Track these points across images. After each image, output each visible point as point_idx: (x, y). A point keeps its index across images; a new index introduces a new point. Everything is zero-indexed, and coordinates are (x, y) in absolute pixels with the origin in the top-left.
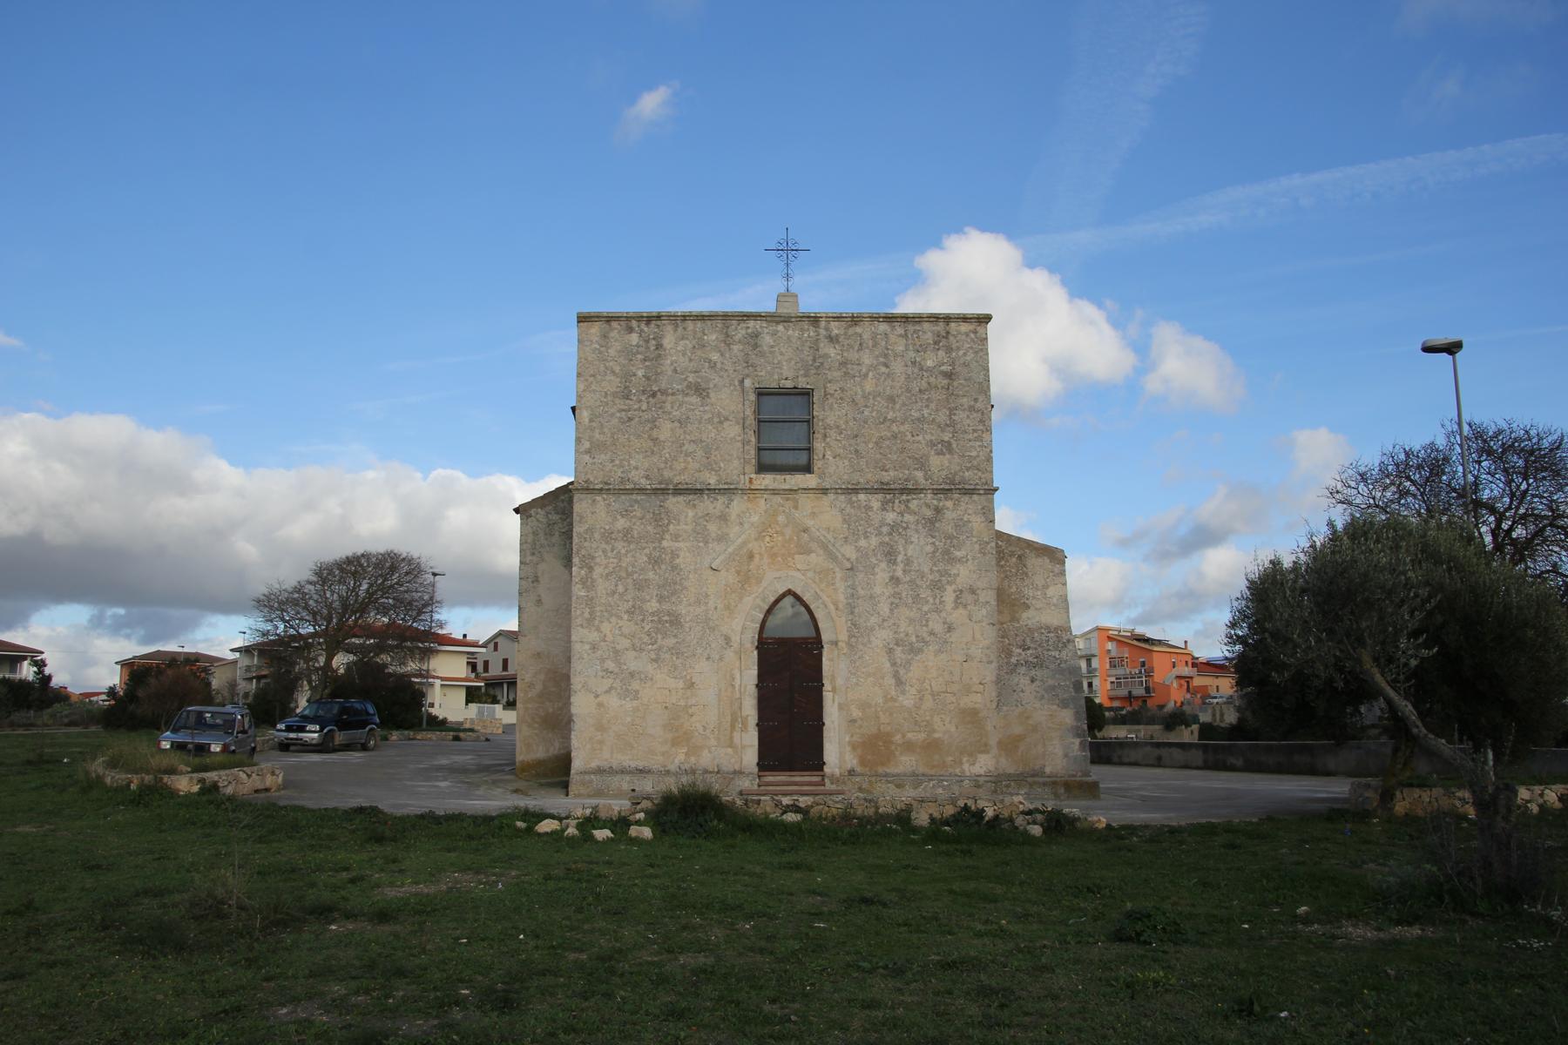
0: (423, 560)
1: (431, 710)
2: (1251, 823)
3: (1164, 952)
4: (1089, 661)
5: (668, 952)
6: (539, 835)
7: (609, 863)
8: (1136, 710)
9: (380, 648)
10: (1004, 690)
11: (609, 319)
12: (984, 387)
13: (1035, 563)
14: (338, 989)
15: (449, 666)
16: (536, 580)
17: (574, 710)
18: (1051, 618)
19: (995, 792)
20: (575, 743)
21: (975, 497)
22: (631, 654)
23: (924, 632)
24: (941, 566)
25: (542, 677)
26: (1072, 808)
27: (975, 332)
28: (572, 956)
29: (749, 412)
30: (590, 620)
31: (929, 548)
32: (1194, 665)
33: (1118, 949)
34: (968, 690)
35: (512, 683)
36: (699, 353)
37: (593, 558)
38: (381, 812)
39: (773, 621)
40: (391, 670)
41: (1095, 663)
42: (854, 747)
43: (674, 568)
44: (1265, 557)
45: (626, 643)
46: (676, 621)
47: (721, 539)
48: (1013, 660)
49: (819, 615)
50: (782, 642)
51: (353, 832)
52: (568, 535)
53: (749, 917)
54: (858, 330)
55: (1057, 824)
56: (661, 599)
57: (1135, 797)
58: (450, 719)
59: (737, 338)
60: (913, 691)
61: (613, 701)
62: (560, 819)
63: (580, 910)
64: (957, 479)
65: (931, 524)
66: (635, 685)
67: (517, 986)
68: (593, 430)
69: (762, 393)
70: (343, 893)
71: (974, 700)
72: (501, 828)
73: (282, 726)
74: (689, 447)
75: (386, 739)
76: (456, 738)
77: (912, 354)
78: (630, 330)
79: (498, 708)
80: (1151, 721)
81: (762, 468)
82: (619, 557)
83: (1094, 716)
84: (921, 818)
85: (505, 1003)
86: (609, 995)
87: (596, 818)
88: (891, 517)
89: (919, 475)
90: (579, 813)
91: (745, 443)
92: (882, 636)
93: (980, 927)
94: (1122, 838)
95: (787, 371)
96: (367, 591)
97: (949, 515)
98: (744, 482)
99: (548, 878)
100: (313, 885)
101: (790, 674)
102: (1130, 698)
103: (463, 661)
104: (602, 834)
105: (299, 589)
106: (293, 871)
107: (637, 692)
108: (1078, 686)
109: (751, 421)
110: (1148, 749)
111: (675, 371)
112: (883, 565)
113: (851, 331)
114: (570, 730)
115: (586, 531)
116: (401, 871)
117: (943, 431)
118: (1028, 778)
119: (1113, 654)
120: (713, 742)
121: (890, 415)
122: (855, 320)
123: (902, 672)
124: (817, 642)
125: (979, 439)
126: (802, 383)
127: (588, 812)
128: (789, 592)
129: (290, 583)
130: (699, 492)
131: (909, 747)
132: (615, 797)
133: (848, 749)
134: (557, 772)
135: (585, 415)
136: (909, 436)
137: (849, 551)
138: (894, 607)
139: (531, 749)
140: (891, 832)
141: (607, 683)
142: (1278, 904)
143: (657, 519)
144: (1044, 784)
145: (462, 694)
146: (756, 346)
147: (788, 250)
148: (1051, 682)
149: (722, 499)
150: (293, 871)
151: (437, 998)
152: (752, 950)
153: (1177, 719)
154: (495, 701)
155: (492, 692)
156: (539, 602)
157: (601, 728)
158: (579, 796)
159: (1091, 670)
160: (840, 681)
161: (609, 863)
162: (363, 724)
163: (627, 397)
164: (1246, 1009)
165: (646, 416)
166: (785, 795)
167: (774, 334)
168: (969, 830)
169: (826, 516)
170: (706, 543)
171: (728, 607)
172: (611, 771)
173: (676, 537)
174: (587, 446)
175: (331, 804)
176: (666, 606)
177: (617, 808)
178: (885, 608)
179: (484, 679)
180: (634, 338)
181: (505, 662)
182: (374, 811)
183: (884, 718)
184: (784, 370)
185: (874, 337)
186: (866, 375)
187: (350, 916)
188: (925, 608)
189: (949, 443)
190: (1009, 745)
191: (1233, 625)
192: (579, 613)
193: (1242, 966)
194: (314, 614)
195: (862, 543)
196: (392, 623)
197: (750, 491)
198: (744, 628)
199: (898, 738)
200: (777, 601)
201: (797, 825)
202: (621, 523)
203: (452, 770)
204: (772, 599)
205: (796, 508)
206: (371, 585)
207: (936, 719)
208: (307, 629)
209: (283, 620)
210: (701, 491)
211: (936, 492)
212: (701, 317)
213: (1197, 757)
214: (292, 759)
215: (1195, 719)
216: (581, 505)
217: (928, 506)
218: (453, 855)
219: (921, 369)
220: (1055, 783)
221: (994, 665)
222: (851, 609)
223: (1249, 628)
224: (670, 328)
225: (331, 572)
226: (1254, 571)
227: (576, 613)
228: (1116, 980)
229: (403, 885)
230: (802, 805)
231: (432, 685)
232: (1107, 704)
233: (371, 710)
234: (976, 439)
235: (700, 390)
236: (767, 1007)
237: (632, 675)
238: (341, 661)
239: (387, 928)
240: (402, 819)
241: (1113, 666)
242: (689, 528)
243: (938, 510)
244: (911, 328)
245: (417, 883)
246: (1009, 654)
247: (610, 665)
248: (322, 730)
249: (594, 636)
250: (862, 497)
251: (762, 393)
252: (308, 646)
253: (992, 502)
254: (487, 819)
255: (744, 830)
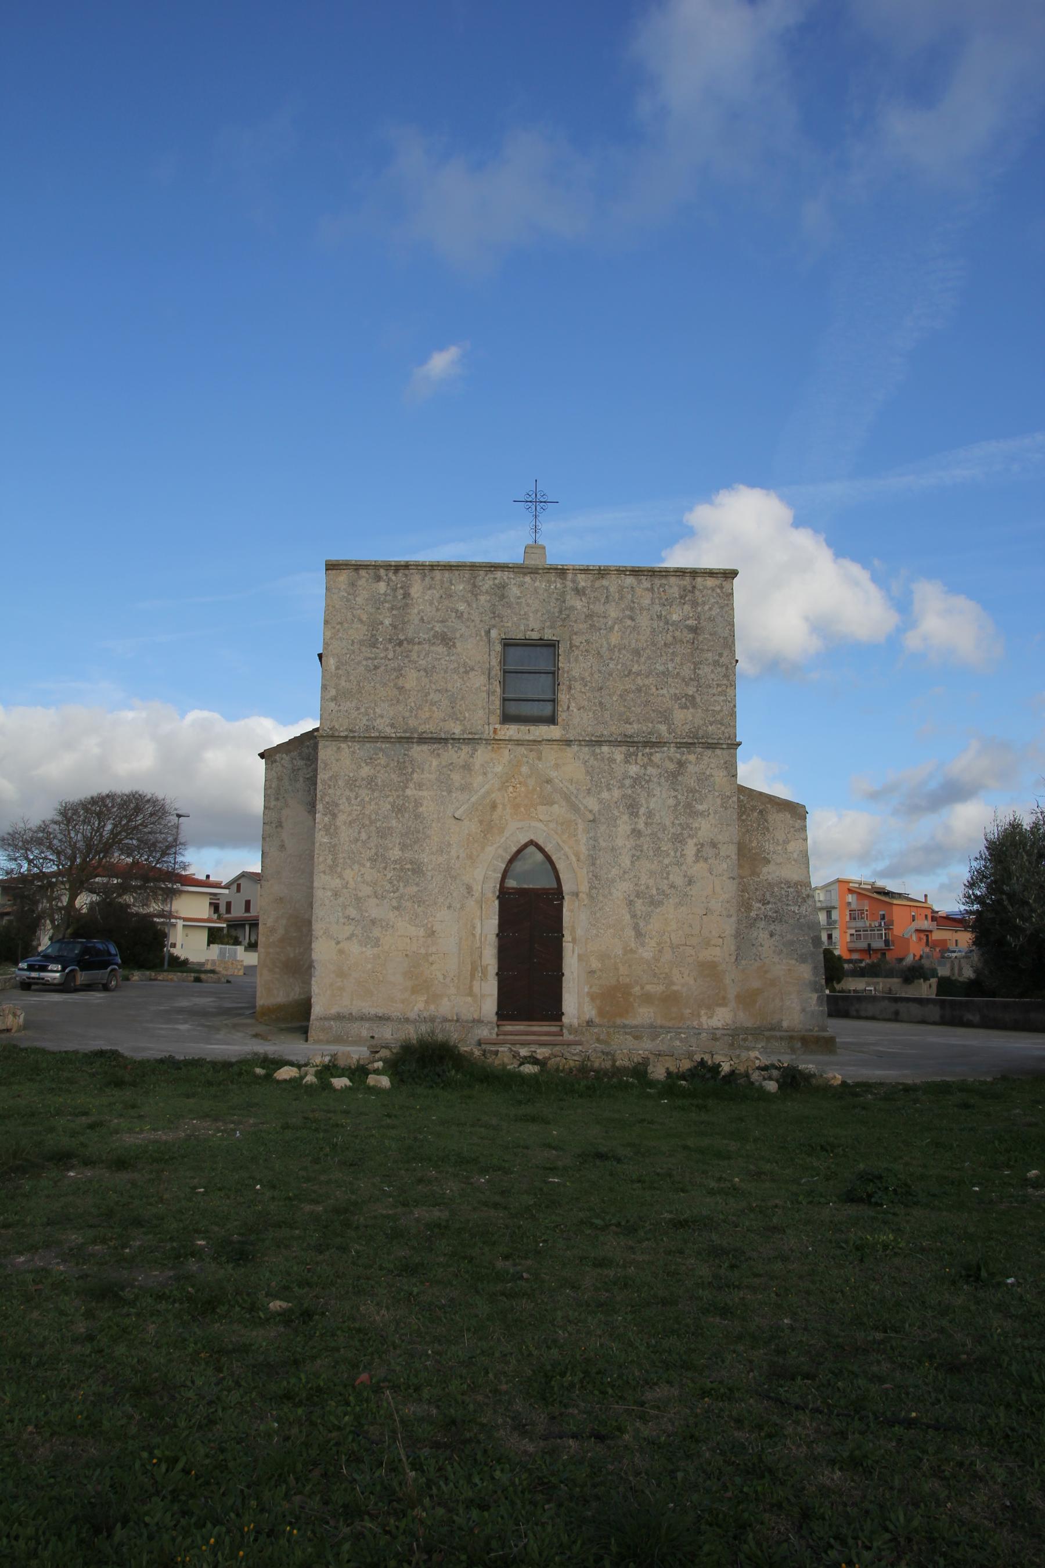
0: (168, 801)
1: (172, 950)
2: (985, 1083)
3: (894, 1214)
4: (829, 912)
5: (404, 1205)
6: (278, 1082)
7: (346, 1112)
8: (876, 962)
9: (124, 889)
10: (743, 942)
11: (357, 567)
12: (729, 643)
13: (776, 818)
14: (75, 1238)
15: (192, 907)
16: (280, 825)
17: (315, 956)
18: (790, 873)
19: (732, 1045)
20: (315, 989)
21: (718, 752)
22: (373, 901)
23: (664, 885)
24: (682, 819)
25: (284, 922)
26: (808, 1065)
27: (721, 587)
28: (308, 1208)
29: (495, 662)
30: (332, 868)
31: (671, 802)
32: (933, 919)
33: (852, 1210)
34: (707, 943)
35: (254, 925)
36: (446, 602)
37: (337, 805)
38: (122, 1056)
39: (519, 866)
40: (134, 910)
41: (835, 915)
42: (593, 998)
43: (417, 816)
44: (1005, 818)
45: (366, 890)
46: (418, 870)
47: (465, 788)
48: (753, 914)
49: (560, 866)
50: (522, 892)
51: (93, 1075)
52: (312, 781)
53: (483, 1171)
54: (605, 582)
55: (792, 1080)
56: (404, 847)
57: (876, 1052)
58: (191, 959)
59: (484, 589)
60: (653, 943)
61: (354, 948)
62: (299, 1067)
63: (316, 1161)
64: (701, 733)
65: (674, 777)
66: (376, 932)
67: (253, 1237)
68: (339, 677)
69: (508, 644)
70: (82, 1139)
71: (713, 954)
72: (240, 1074)
73: (24, 965)
74: (432, 696)
75: (127, 979)
76: (198, 980)
77: (657, 608)
78: (378, 579)
79: (240, 949)
80: (890, 974)
81: (507, 718)
82: (363, 804)
83: (833, 968)
84: (658, 1072)
85: (241, 1256)
86: (344, 1249)
87: (335, 1066)
88: (634, 770)
89: (663, 728)
90: (318, 1060)
91: (489, 693)
92: (621, 889)
93: (713, 1184)
94: (856, 1095)
95: (534, 622)
96: (112, 831)
97: (691, 768)
98: (488, 732)
99: (286, 1127)
100: (52, 1130)
101: (530, 926)
102: (869, 950)
103: (206, 902)
104: (340, 1082)
105: (43, 828)
106: (33, 1115)
107: (378, 939)
108: (817, 941)
109: (497, 671)
110: (886, 1003)
111: (422, 620)
112: (625, 817)
113: (597, 584)
114: (311, 976)
115: (330, 779)
116: (140, 1117)
117: (687, 685)
118: (765, 1032)
119: (854, 906)
120: (453, 990)
121: (635, 668)
122: (602, 572)
123: (642, 924)
124: (558, 893)
125: (723, 693)
126: (548, 635)
127: (327, 1059)
128: (531, 843)
129: (35, 822)
130: (443, 741)
131: (647, 999)
132: (355, 1043)
133: (587, 999)
134: (297, 1017)
135: (332, 662)
136: (654, 689)
137: (592, 803)
138: (635, 859)
139: (272, 992)
140: (627, 1086)
141: (348, 930)
142: (1009, 1167)
143: (401, 767)
144: (781, 1038)
145: (204, 936)
146: (503, 597)
147: (536, 503)
148: (789, 937)
149: (466, 749)
150: (33, 1115)
151: (173, 1249)
152: (485, 1204)
153: (914, 973)
154: (237, 942)
155: (234, 933)
156: (282, 847)
157: (341, 974)
158: (318, 1041)
159: (830, 922)
160: (579, 932)
161: (346, 1112)
162: (104, 965)
163: (374, 645)
164: (973, 1274)
165: (393, 664)
166: (524, 1044)
167: (521, 585)
168: (706, 1086)
169: (569, 768)
170: (450, 792)
171: (470, 857)
172: (351, 1018)
173: (420, 786)
174: (333, 692)
175: (70, 1046)
176: (408, 855)
177: (355, 1057)
178: (626, 862)
179: (226, 920)
180: (382, 587)
181: (248, 903)
182: (114, 1054)
183: (623, 970)
184: (530, 619)
185: (621, 588)
186: (612, 628)
187: (88, 1162)
188: (666, 861)
189: (693, 697)
190: (747, 999)
191: (972, 885)
192: (322, 860)
193: (971, 1229)
194: (58, 853)
195: (605, 795)
196: (136, 863)
197: (495, 742)
198: (486, 878)
199: (637, 990)
200: (519, 851)
201: (534, 1077)
202: (366, 771)
203: (194, 1013)
204: (514, 849)
205: (540, 759)
206: (115, 826)
207: (675, 971)
208: (51, 868)
209: (27, 858)
210: (445, 741)
211: (679, 745)
212: (449, 567)
213: (935, 1012)
214: (34, 998)
215: (934, 973)
216: (326, 752)
217: (671, 759)
218: (192, 1100)
219: (667, 623)
220: (791, 1038)
221: (734, 919)
222: (593, 861)
223: (987, 888)
224: (417, 577)
225: (75, 812)
226: (994, 833)
227: (319, 859)
228: (846, 1242)
229: (142, 1131)
230: (539, 1057)
231: (174, 925)
232: (846, 956)
233: (113, 950)
234: (720, 694)
235: (446, 640)
236: (500, 1264)
237: (373, 922)
238: (84, 901)
239: (124, 1176)
240: (142, 1063)
241: (853, 918)
242: (433, 777)
243: (681, 764)
244: (657, 582)
245: (155, 1130)
246: (749, 908)
247: (352, 912)
248: (63, 970)
249: (337, 882)
250: (605, 749)
251: (508, 644)
252: (52, 885)
253: (734, 756)
254: (227, 1065)
255: (482, 1081)
